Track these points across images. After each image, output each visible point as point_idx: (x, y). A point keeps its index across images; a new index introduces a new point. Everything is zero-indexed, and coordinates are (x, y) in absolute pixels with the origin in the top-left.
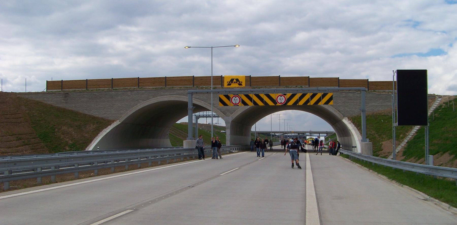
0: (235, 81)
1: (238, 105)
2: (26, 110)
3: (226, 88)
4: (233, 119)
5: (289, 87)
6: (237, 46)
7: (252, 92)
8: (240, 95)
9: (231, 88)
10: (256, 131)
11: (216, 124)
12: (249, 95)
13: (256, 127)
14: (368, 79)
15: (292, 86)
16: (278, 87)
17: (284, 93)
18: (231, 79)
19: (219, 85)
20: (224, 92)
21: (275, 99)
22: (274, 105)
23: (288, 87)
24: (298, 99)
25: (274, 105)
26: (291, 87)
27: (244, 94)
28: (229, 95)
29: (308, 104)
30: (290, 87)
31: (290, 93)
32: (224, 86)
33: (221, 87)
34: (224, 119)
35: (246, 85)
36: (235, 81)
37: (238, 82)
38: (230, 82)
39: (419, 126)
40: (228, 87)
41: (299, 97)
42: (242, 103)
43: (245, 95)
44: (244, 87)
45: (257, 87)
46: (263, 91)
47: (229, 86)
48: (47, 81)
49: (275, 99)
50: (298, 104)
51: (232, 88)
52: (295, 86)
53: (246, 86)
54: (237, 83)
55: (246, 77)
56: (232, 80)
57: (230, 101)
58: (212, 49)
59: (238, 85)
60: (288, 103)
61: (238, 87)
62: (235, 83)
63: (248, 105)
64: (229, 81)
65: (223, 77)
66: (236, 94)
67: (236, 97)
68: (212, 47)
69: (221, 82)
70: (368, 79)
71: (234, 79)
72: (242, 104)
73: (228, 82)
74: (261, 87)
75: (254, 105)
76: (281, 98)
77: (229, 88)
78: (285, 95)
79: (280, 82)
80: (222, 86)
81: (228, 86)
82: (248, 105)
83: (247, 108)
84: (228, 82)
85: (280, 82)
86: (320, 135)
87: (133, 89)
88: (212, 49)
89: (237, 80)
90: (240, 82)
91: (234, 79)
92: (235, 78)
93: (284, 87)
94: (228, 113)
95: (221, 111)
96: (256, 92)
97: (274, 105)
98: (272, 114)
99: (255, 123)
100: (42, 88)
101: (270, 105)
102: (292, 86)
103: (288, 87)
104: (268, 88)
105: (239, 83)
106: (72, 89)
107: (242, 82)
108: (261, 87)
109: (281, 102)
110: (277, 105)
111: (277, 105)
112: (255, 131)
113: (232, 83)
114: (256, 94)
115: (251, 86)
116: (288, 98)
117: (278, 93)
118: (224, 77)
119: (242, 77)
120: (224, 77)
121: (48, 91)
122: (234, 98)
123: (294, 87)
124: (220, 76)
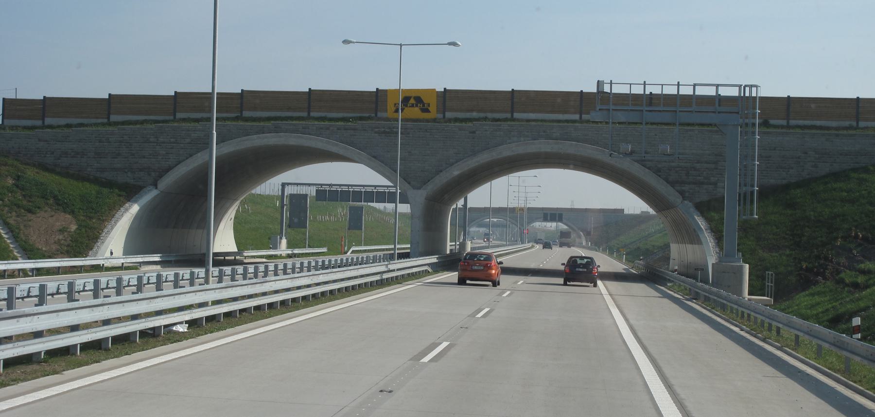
0: (412, 101)
37: (419, 105)
54: (417, 106)
62: (412, 106)
90: (424, 105)
92: (414, 95)
105: (421, 106)
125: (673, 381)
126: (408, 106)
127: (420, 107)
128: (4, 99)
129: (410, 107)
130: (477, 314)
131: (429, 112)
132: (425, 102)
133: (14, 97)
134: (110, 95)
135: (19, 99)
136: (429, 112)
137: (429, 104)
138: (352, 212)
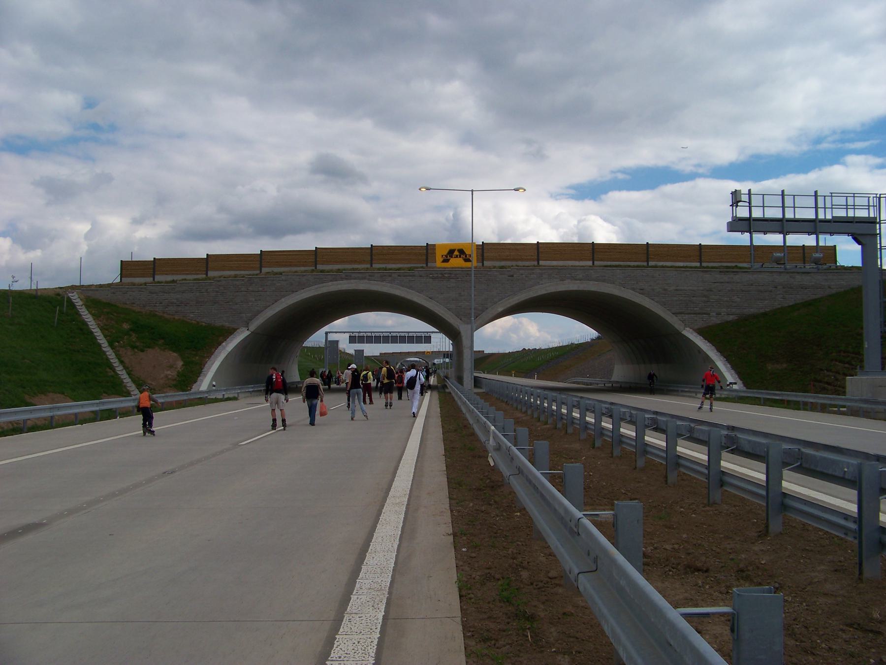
0: (456, 253)
6: (521, 190)
14: (835, 246)
18: (448, 250)
37: (462, 256)
38: (446, 256)
48: (121, 261)
54: (460, 257)
56: (451, 252)
58: (472, 195)
62: (457, 257)
64: (445, 254)
68: (472, 191)
70: (835, 246)
71: (455, 250)
73: (442, 256)
84: (442, 256)
86: (595, 264)
87: (193, 281)
88: (472, 195)
89: (461, 252)
90: (466, 256)
91: (455, 250)
100: (111, 275)
105: (464, 256)
106: (304, 266)
107: (470, 256)
121: (125, 280)
124: (801, 246)
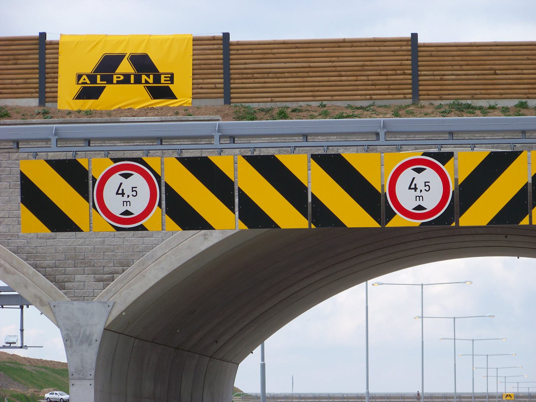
0: (126, 67)
1: (142, 228)
2: (89, 235)
3: (69, 113)
4: (115, 313)
5: (475, 108)
7: (233, 138)
8: (153, 162)
9: (101, 113)
10: (474, 392)
11: (10, 345)
12: (216, 160)
13: (263, 366)
15: (492, 102)
16: (401, 108)
17: (435, 150)
19: (26, 95)
20: (217, 135)
21: (383, 186)
22: (377, 225)
23: (469, 107)
24: (527, 184)
25: (370, 222)
26: (484, 111)
27: (186, 154)
28: (83, 162)
29: (452, 225)
30: (481, 108)
31: (473, 147)
32: (55, 99)
33: (41, 110)
34: (54, 314)
35: (195, 96)
36: (126, 67)
37: (144, 77)
38: (92, 78)
39: (260, 345)
40: (79, 112)
41: (19, 198)
42: (168, 213)
43: (190, 163)
44: (186, 109)
45: (269, 105)
46: (305, 136)
47: (88, 104)
49: (380, 190)
50: (525, 221)
51: (109, 114)
52: (516, 102)
53: (198, 102)
54: (138, 81)
55: (197, 41)
57: (87, 199)
59: (146, 95)
60: (463, 210)
61: (146, 111)
62: (126, 80)
63: (206, 226)
65: (51, 43)
66: (128, 155)
67: (126, 176)
69: (34, 79)
72: (167, 219)
74: (294, 105)
75: (244, 227)
76: (420, 179)
77: (89, 113)
78: (445, 157)
79: (415, 75)
80: (42, 102)
81: (81, 101)
82: (206, 226)
83: (203, 248)
84: (79, 77)
85: (415, 75)
90: (157, 79)
92: (129, 51)
93: (440, 106)
94: (78, 277)
95: (35, 266)
96: (255, 143)
97: (370, 222)
98: (370, 282)
99: (260, 339)
101: (348, 227)
102: (492, 102)
103: (470, 109)
104: (341, 117)
105: (151, 80)
108: (294, 111)
109: (420, 208)
110: (391, 224)
111: (391, 224)
112: (472, 392)
113: (110, 82)
114: (256, 153)
115: (228, 100)
116: (460, 182)
117: (399, 148)
118: (55, 44)
119: (173, 41)
120: (57, 43)
122: (116, 179)
123: (505, 111)
125: (192, 235)
126: (115, 80)
127: (147, 82)
128: (173, 84)
129: (119, 82)
130: (379, 227)
131: (172, 96)
132: (161, 69)
133: (361, 390)
134: (412, 34)
135: (312, 213)
136: (172, 96)
137: (172, 75)
138: (74, 227)
